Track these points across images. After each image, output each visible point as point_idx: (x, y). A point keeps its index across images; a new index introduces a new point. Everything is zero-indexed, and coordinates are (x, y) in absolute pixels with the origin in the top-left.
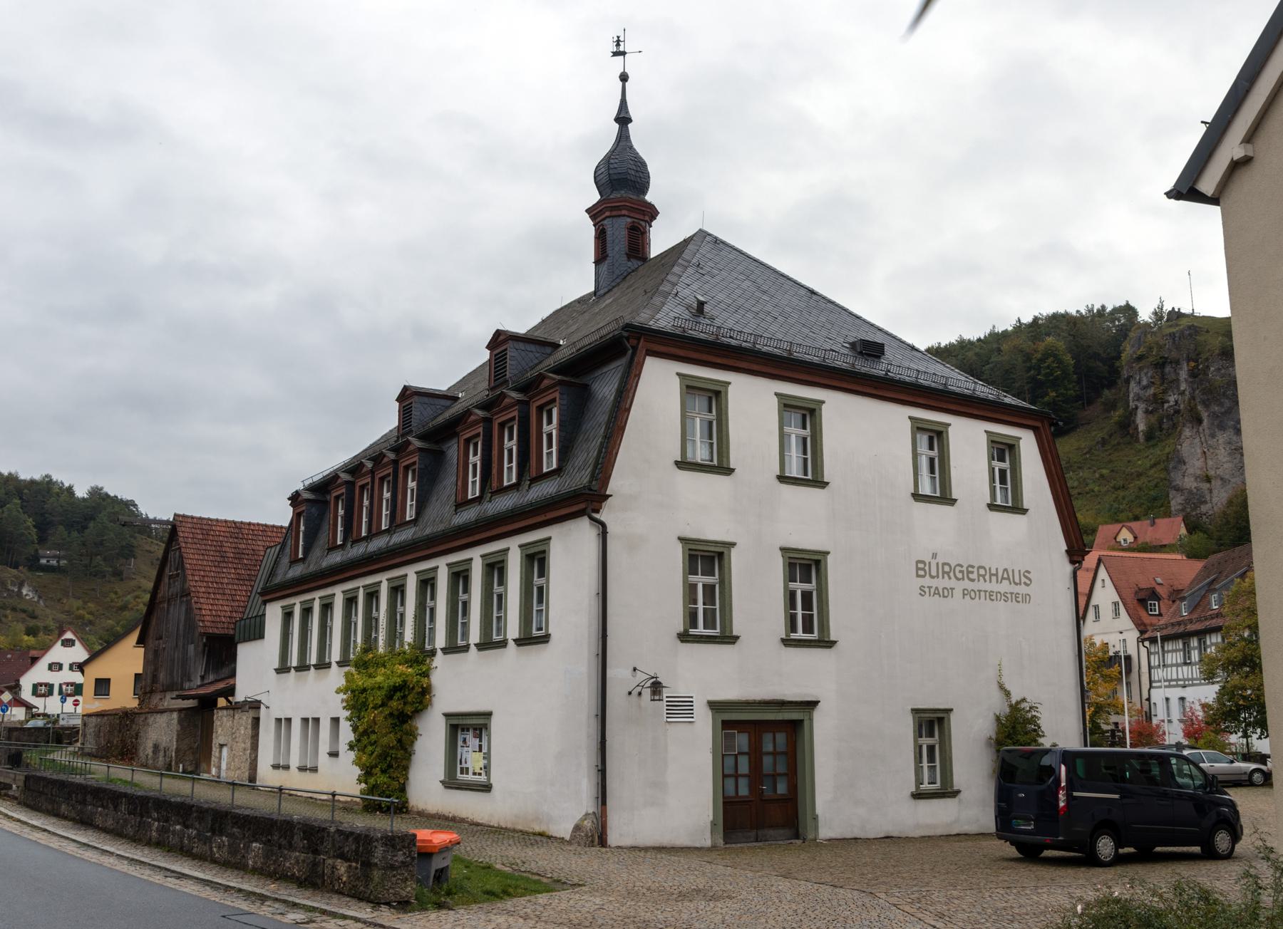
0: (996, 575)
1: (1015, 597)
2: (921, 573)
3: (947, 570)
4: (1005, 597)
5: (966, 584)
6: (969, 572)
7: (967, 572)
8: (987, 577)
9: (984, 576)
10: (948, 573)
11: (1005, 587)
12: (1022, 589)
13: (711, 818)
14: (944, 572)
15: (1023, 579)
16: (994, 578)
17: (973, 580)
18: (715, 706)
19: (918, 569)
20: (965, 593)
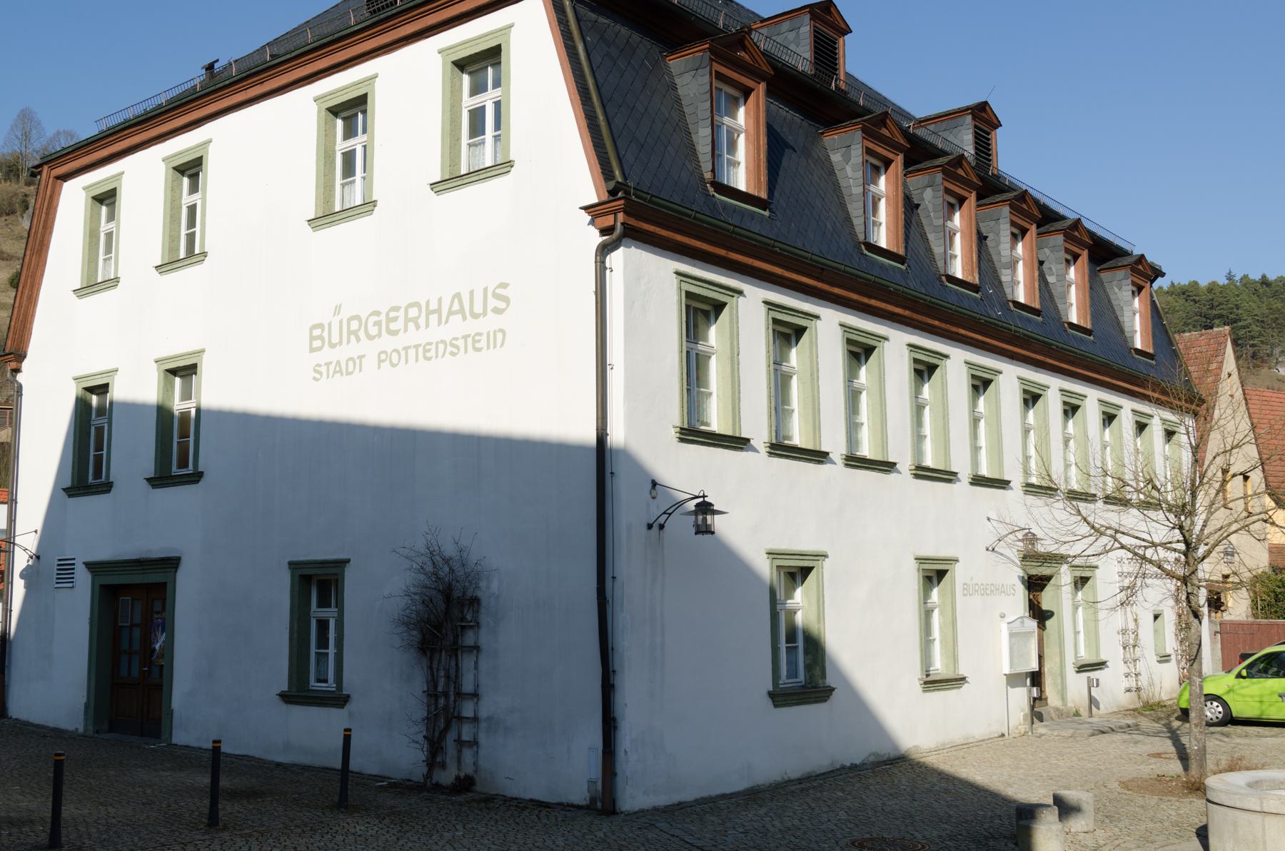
0: (439, 311)
1: (473, 342)
2: (317, 344)
3: (355, 328)
4: (452, 348)
5: (387, 342)
6: (389, 320)
7: (386, 322)
8: (422, 321)
9: (415, 320)
10: (355, 333)
11: (457, 327)
12: (490, 323)
13: (85, 700)
14: (350, 333)
15: (492, 302)
17: (394, 333)
18: (90, 566)
19: (312, 338)
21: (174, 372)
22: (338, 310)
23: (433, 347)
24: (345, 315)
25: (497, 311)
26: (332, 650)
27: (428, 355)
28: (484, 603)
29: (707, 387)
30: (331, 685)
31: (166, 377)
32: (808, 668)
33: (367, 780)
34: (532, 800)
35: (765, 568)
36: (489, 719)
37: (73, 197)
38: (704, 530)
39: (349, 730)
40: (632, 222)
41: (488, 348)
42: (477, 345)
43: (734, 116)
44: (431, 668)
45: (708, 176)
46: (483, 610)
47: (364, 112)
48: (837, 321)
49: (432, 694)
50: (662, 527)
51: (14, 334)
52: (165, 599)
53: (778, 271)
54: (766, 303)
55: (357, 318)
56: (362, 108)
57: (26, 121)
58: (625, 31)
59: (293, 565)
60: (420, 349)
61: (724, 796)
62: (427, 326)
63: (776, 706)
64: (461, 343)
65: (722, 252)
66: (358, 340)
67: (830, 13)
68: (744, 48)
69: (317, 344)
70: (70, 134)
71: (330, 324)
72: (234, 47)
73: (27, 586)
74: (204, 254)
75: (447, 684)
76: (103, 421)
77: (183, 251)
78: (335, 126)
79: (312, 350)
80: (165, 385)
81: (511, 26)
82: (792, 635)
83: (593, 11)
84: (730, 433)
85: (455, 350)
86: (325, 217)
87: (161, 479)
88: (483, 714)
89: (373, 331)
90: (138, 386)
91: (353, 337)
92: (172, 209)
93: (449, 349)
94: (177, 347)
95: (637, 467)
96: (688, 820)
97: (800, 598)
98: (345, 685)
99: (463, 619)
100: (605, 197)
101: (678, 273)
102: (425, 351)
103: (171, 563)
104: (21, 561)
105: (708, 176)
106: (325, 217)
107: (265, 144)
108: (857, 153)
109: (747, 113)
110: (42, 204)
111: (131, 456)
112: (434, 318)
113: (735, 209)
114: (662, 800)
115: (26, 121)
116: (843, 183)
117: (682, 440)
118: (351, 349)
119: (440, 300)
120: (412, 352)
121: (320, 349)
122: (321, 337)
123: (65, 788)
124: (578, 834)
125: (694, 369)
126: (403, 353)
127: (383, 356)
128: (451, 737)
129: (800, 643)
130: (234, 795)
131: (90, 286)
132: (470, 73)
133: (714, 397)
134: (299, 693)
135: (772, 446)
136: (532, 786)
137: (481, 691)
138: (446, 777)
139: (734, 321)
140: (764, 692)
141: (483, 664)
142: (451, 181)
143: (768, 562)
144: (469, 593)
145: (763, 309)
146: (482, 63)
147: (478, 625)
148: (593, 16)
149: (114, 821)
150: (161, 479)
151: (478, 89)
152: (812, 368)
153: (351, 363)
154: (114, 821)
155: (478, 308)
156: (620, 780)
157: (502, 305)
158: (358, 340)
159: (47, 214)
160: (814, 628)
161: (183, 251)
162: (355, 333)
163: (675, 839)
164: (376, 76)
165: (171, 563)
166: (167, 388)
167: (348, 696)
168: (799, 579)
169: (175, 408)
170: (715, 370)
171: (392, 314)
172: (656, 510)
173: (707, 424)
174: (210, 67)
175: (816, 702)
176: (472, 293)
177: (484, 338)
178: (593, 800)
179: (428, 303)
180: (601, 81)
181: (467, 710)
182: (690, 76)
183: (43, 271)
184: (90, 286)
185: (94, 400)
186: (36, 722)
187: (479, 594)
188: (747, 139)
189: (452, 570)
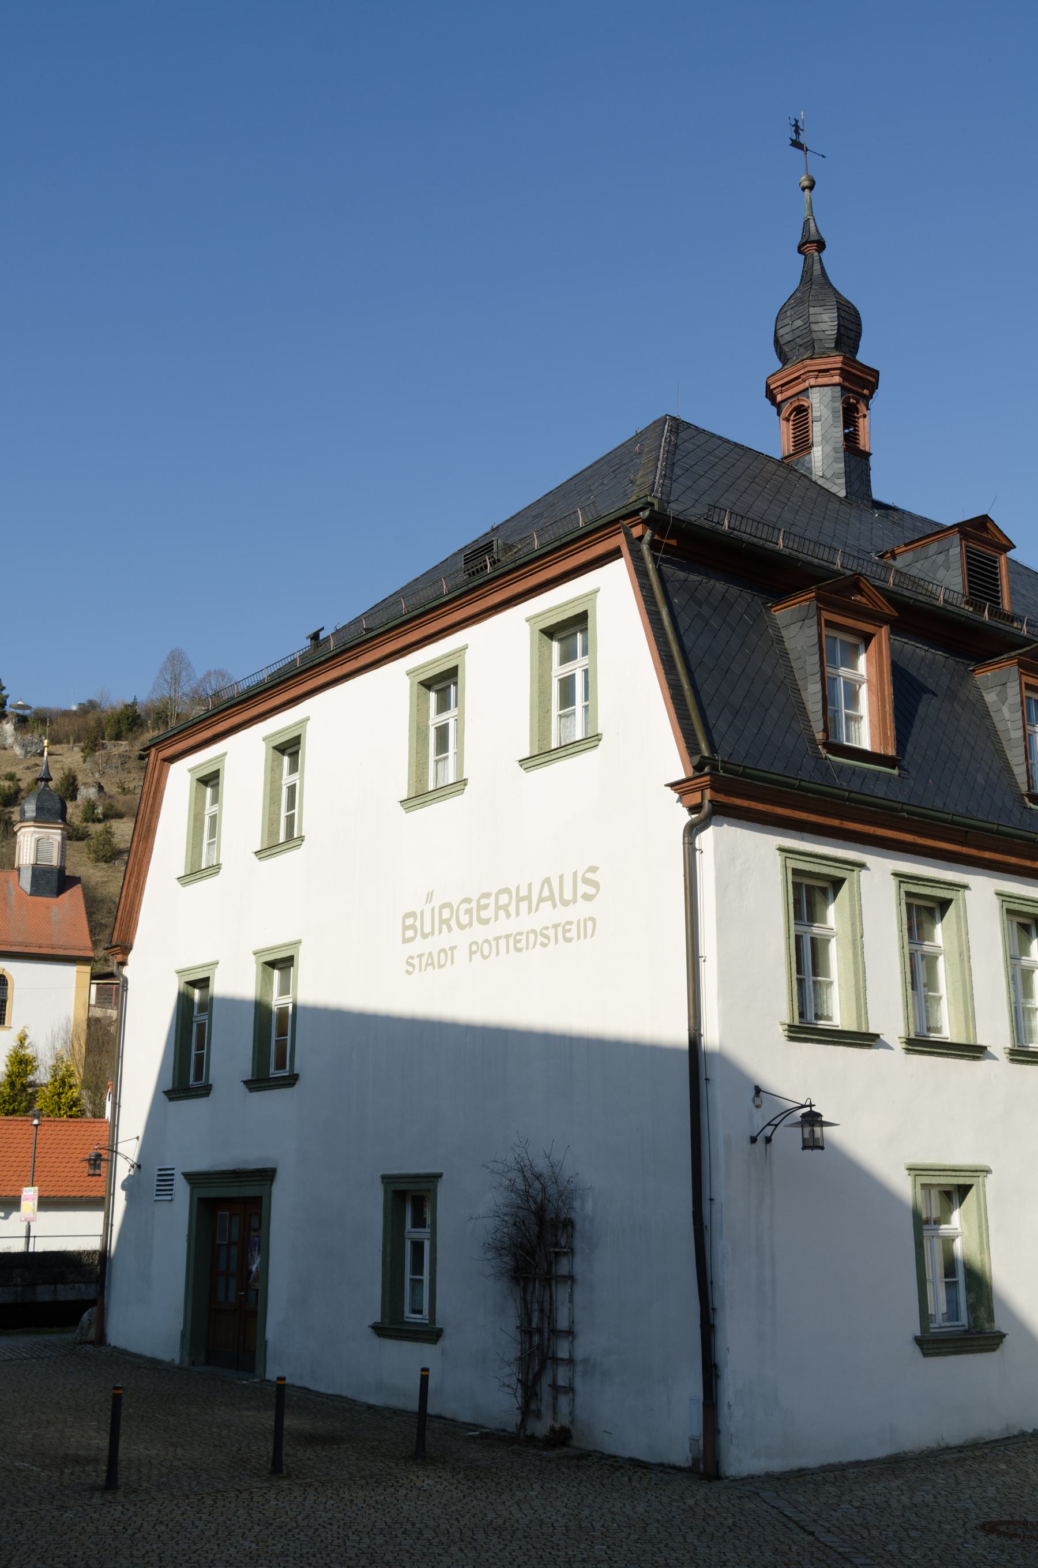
0: (528, 898)
1: (563, 931)
2: (410, 934)
3: (447, 916)
4: (542, 937)
5: (479, 933)
7: (477, 909)
8: (512, 909)
9: (505, 908)
10: (447, 922)
11: (547, 915)
12: (581, 910)
13: (181, 1327)
14: (442, 922)
15: (583, 888)
16: (524, 905)
17: (485, 922)
18: (188, 1176)
19: (405, 928)
20: (475, 948)
21: (272, 964)
22: (430, 897)
23: (524, 937)
24: (437, 903)
25: (587, 897)
26: (426, 1277)
27: (519, 946)
28: (578, 1227)
29: (827, 975)
30: (423, 1318)
31: (264, 971)
32: (972, 1308)
33: (451, 1426)
34: (631, 1459)
35: (905, 1187)
36: (586, 1361)
37: (180, 778)
38: (813, 1144)
39: (427, 1370)
40: (722, 798)
41: (579, 938)
42: (568, 935)
43: (853, 666)
44: (524, 1300)
45: (820, 736)
46: (577, 1235)
47: (456, 684)
48: (992, 890)
49: (526, 1330)
50: (768, 1140)
51: (121, 925)
52: (260, 1215)
53: (908, 838)
54: (896, 875)
55: (448, 905)
56: (453, 680)
57: (176, 662)
58: (720, 586)
59: (386, 1179)
60: (511, 940)
61: (858, 1464)
62: (518, 914)
63: (925, 1355)
64: (551, 933)
65: (835, 822)
66: (450, 930)
67: (986, 529)
68: (860, 591)
69: (410, 934)
70: (221, 674)
71: (422, 912)
72: (335, 615)
73: (129, 1199)
74: (301, 838)
75: (541, 1319)
76: (203, 1017)
77: (282, 836)
78: (428, 700)
79: (405, 941)
80: (263, 979)
81: (597, 591)
82: (950, 1266)
83: (682, 569)
84: (853, 1028)
85: (546, 941)
86: (419, 797)
87: (259, 1082)
88: (579, 1355)
89: (464, 919)
90: (237, 982)
91: (444, 927)
92: (272, 790)
93: (540, 939)
94: (274, 938)
95: (735, 1072)
96: (801, 1490)
97: (958, 1222)
98: (437, 1317)
99: (557, 1244)
100: (691, 772)
101: (781, 850)
102: (516, 941)
103: (266, 1175)
104: (123, 1170)
105: (820, 736)
106: (419, 797)
107: (362, 717)
108: (1013, 691)
109: (868, 660)
110: (150, 787)
111: (230, 1056)
112: (524, 905)
113: (854, 770)
114: (777, 1465)
115: (176, 662)
116: (1000, 727)
117: (791, 1039)
118: (442, 940)
119: (530, 885)
120: (502, 942)
121: (412, 939)
122: (413, 927)
123: (122, 1422)
124: (665, 1500)
125: (808, 960)
126: (494, 944)
127: (474, 948)
128: (546, 1380)
129: (961, 1277)
130: (309, 1440)
131: (196, 872)
132: (560, 640)
133: (836, 985)
134: (392, 1326)
135: (909, 1041)
136: (631, 1443)
137: (578, 1328)
138: (540, 1428)
139: (856, 899)
140: (910, 1338)
141: (578, 1297)
142: (541, 756)
143: (909, 1180)
144: (563, 1216)
145: (893, 882)
146: (569, 630)
147: (572, 1252)
148: (682, 575)
149: (178, 1464)
150: (259, 1082)
151: (568, 656)
152: (960, 946)
153: (442, 955)
154: (178, 1464)
155: (568, 895)
156: (723, 1439)
157: (591, 891)
158: (450, 930)
159: (154, 798)
160: (976, 1260)
161: (282, 836)
162: (447, 922)
163: (773, 1512)
164: (465, 648)
165: (266, 1175)
166: (265, 982)
167: (441, 1330)
168: (956, 1198)
169: (274, 1003)
170: (836, 956)
171: (483, 902)
172: (760, 1119)
173: (829, 1018)
174: (315, 637)
175: (981, 1351)
176: (561, 877)
177: (574, 927)
178: (695, 1461)
179: (518, 889)
180: (688, 644)
181: (563, 1353)
182: (796, 627)
183: (150, 858)
184: (196, 872)
185: (197, 994)
186: (134, 1351)
187: (573, 1215)
188: (869, 690)
189: (544, 1189)
